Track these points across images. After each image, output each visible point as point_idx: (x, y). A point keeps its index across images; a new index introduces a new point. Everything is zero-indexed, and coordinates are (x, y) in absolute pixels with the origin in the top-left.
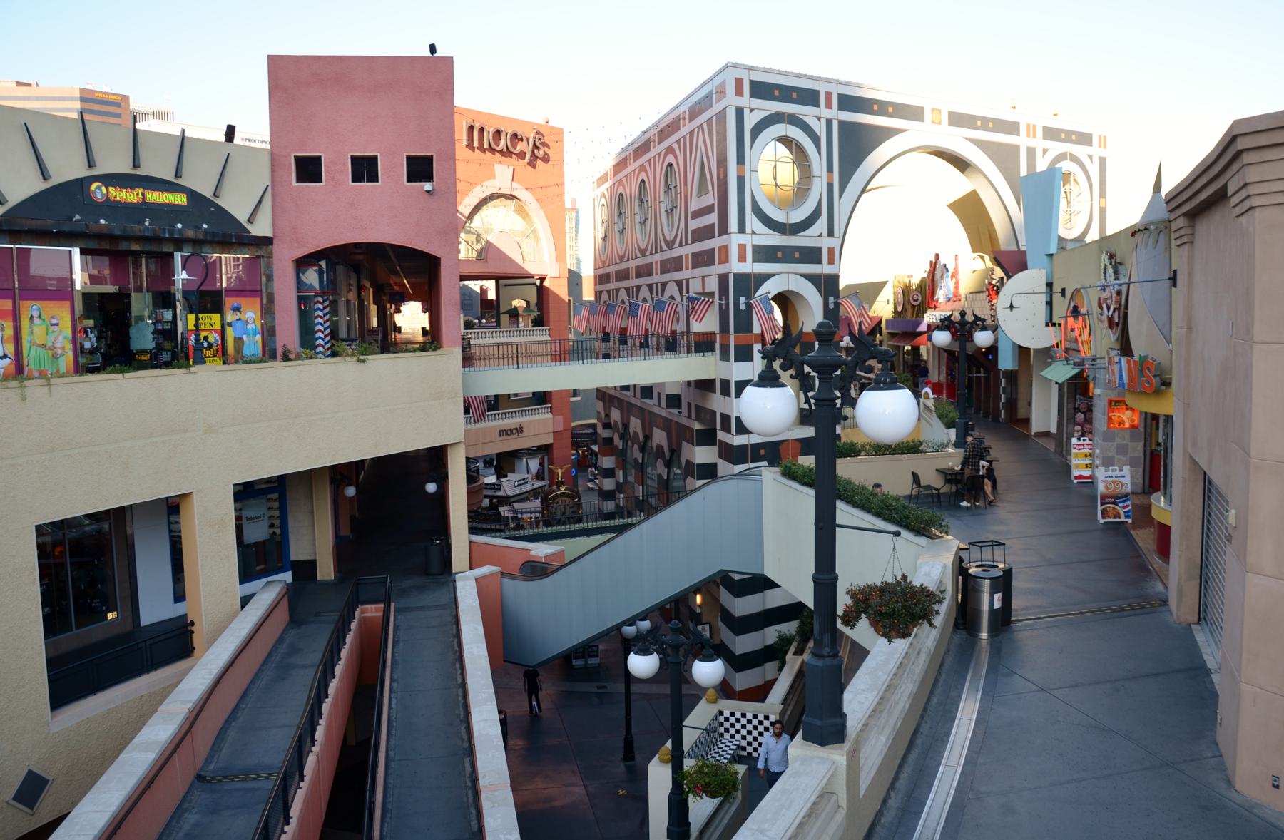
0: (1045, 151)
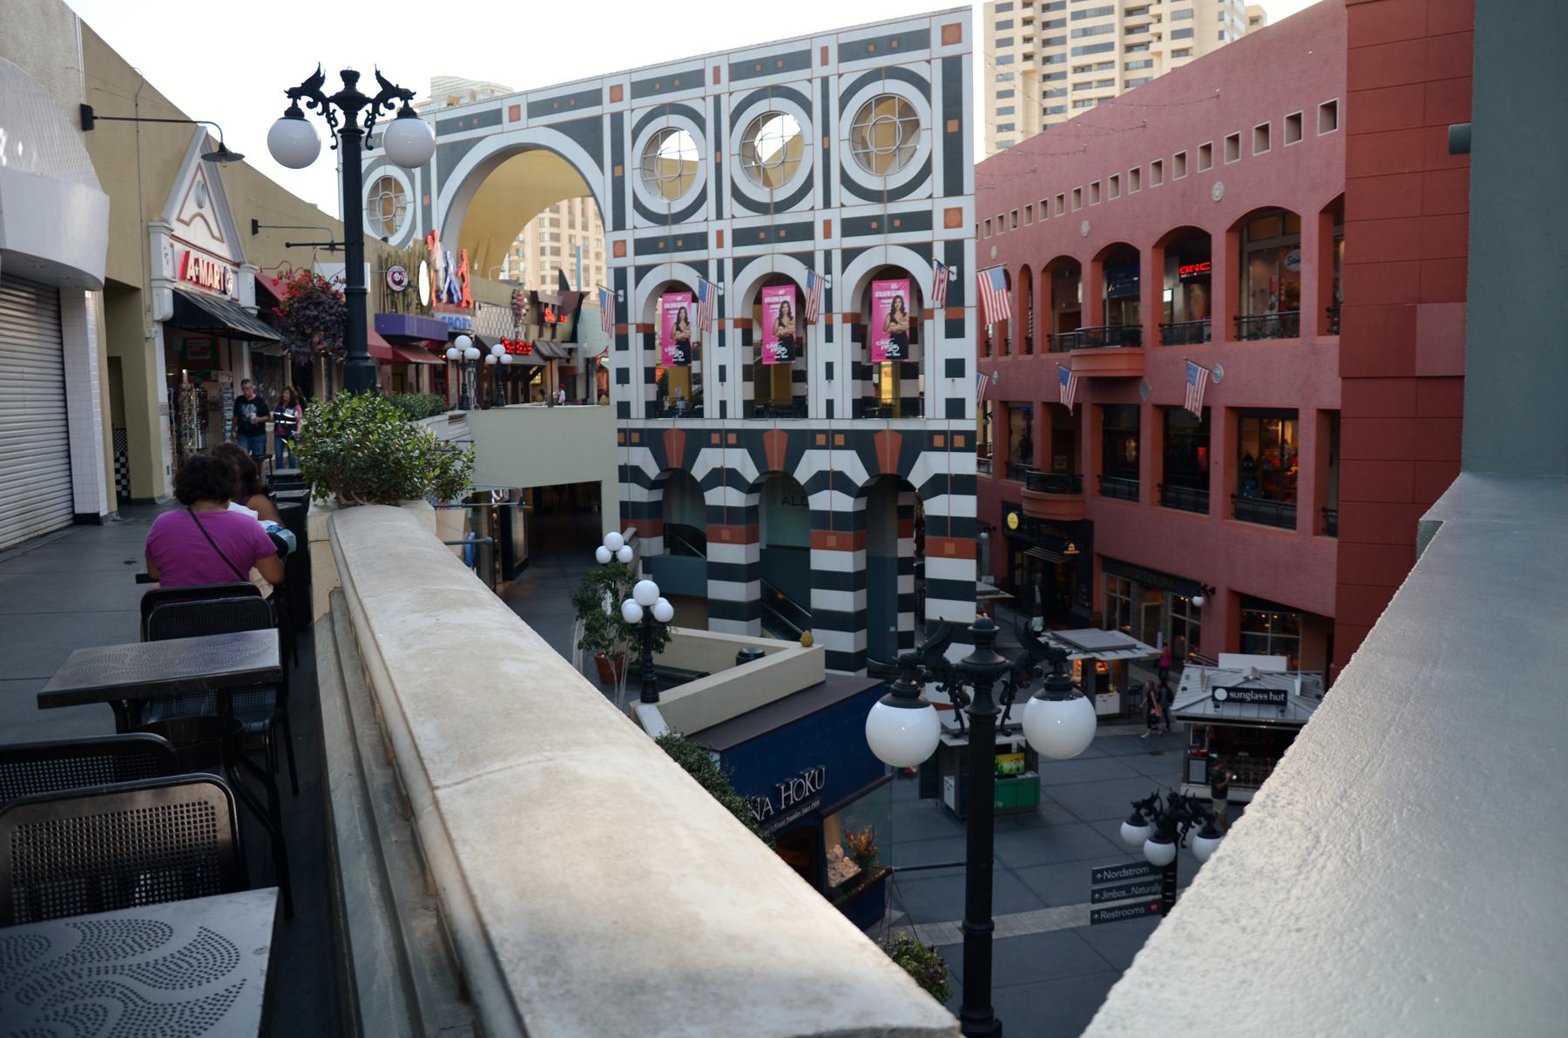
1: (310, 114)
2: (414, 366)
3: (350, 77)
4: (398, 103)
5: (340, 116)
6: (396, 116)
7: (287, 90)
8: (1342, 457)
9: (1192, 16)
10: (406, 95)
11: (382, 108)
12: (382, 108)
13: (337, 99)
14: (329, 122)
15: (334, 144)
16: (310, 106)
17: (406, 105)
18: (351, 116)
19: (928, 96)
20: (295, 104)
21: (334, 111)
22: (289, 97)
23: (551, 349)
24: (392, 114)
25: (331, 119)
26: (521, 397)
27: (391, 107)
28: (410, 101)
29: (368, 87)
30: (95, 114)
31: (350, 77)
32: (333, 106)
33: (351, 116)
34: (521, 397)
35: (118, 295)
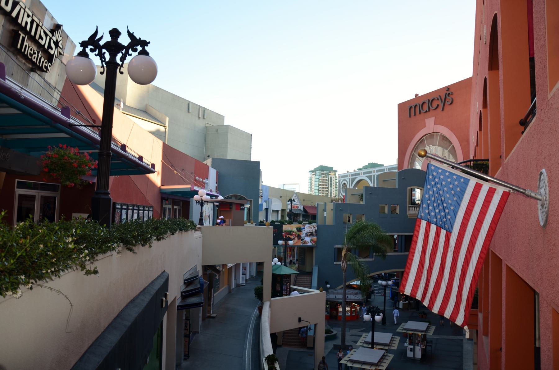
0: (341, 180)
1: (92, 55)
2: (427, 347)
3: (115, 33)
4: (139, 48)
5: (107, 57)
6: (137, 54)
7: (81, 42)
8: (341, 332)
9: (414, 116)
10: (144, 43)
11: (130, 52)
12: (130, 52)
13: (107, 46)
14: (101, 59)
15: (102, 71)
16: (92, 50)
17: (144, 49)
18: (113, 56)
19: (356, 178)
20: (84, 50)
21: (105, 53)
22: (81, 46)
23: (60, 41)
24: (135, 54)
25: (101, 55)
26: (185, 355)
27: (135, 50)
28: (146, 47)
29: (124, 40)
30: (302, 319)
31: (115, 33)
32: (104, 51)
33: (113, 56)
34: (185, 355)
35: (49, 260)
